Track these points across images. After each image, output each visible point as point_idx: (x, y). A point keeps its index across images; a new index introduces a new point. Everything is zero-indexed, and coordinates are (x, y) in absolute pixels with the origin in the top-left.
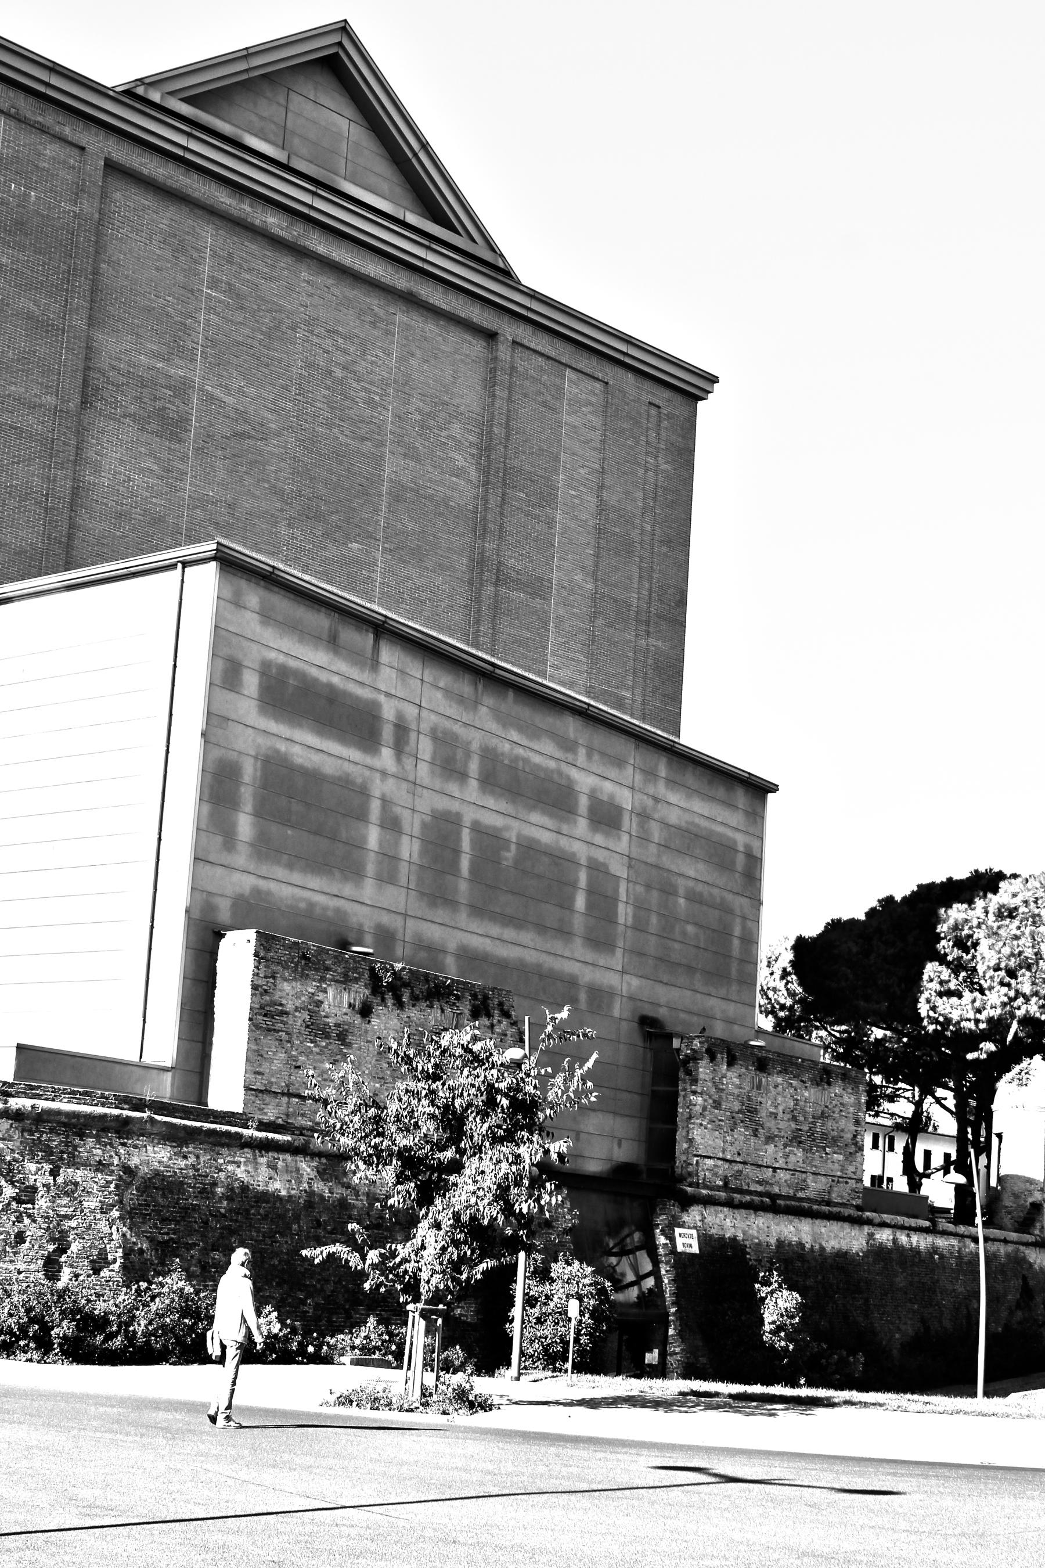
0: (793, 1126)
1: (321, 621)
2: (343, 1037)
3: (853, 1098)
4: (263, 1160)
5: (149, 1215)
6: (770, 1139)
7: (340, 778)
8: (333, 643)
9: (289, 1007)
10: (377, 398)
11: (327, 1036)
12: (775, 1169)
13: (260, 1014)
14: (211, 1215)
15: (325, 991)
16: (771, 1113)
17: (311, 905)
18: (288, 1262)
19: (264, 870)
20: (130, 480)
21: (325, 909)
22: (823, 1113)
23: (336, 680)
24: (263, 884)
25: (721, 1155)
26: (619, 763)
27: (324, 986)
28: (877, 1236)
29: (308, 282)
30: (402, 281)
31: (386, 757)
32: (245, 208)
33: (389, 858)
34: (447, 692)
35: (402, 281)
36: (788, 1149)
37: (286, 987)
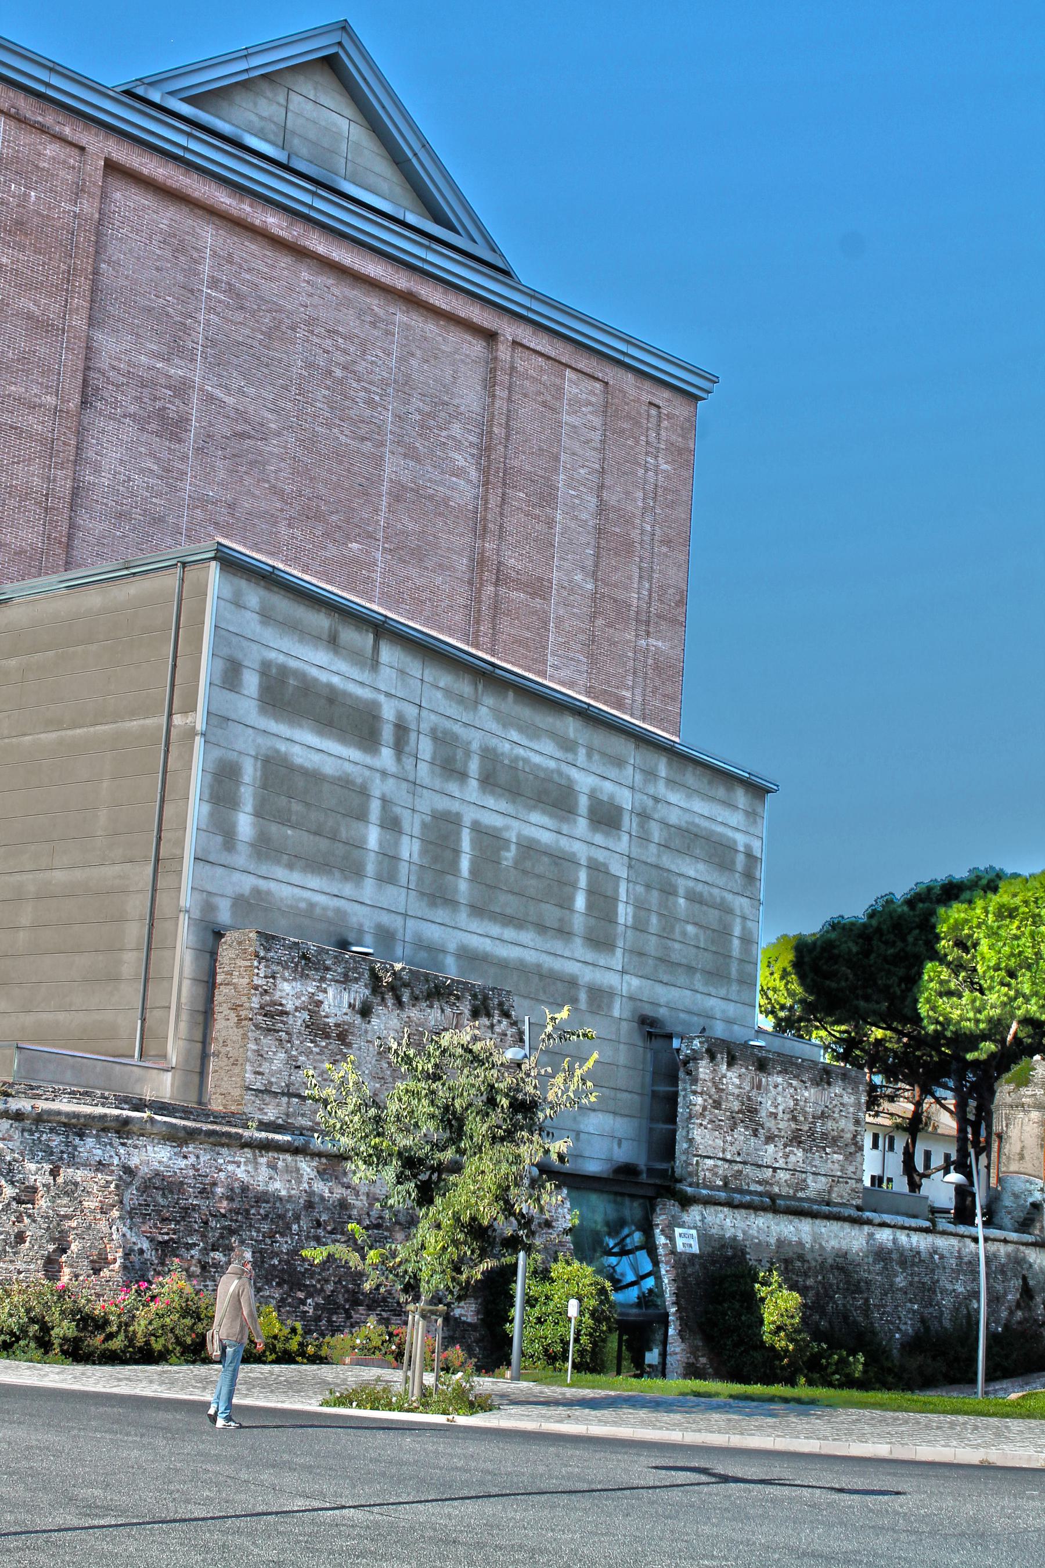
0: (793, 1126)
1: (321, 621)
2: (343, 1036)
3: (853, 1098)
4: (263, 1160)
5: (150, 1215)
6: (770, 1139)
7: (339, 779)
8: (333, 642)
9: (289, 1007)
10: (377, 398)
11: (327, 1036)
12: (775, 1169)
13: (260, 1014)
14: (212, 1215)
15: (325, 991)
16: (772, 1113)
17: (312, 905)
18: (287, 1262)
19: (264, 870)
20: (129, 480)
21: (325, 909)
22: (823, 1113)
23: (336, 680)
24: (263, 884)
25: (721, 1155)
26: (619, 762)
27: (324, 986)
28: (877, 1236)
29: (308, 282)
30: (402, 281)
31: (386, 757)
32: (245, 209)
33: (390, 858)
34: (448, 693)
35: (402, 281)
36: (788, 1149)
37: (286, 987)
